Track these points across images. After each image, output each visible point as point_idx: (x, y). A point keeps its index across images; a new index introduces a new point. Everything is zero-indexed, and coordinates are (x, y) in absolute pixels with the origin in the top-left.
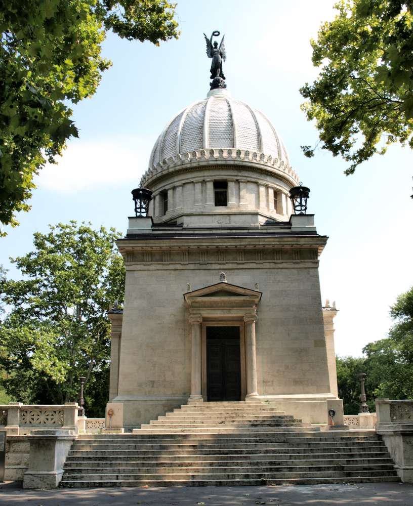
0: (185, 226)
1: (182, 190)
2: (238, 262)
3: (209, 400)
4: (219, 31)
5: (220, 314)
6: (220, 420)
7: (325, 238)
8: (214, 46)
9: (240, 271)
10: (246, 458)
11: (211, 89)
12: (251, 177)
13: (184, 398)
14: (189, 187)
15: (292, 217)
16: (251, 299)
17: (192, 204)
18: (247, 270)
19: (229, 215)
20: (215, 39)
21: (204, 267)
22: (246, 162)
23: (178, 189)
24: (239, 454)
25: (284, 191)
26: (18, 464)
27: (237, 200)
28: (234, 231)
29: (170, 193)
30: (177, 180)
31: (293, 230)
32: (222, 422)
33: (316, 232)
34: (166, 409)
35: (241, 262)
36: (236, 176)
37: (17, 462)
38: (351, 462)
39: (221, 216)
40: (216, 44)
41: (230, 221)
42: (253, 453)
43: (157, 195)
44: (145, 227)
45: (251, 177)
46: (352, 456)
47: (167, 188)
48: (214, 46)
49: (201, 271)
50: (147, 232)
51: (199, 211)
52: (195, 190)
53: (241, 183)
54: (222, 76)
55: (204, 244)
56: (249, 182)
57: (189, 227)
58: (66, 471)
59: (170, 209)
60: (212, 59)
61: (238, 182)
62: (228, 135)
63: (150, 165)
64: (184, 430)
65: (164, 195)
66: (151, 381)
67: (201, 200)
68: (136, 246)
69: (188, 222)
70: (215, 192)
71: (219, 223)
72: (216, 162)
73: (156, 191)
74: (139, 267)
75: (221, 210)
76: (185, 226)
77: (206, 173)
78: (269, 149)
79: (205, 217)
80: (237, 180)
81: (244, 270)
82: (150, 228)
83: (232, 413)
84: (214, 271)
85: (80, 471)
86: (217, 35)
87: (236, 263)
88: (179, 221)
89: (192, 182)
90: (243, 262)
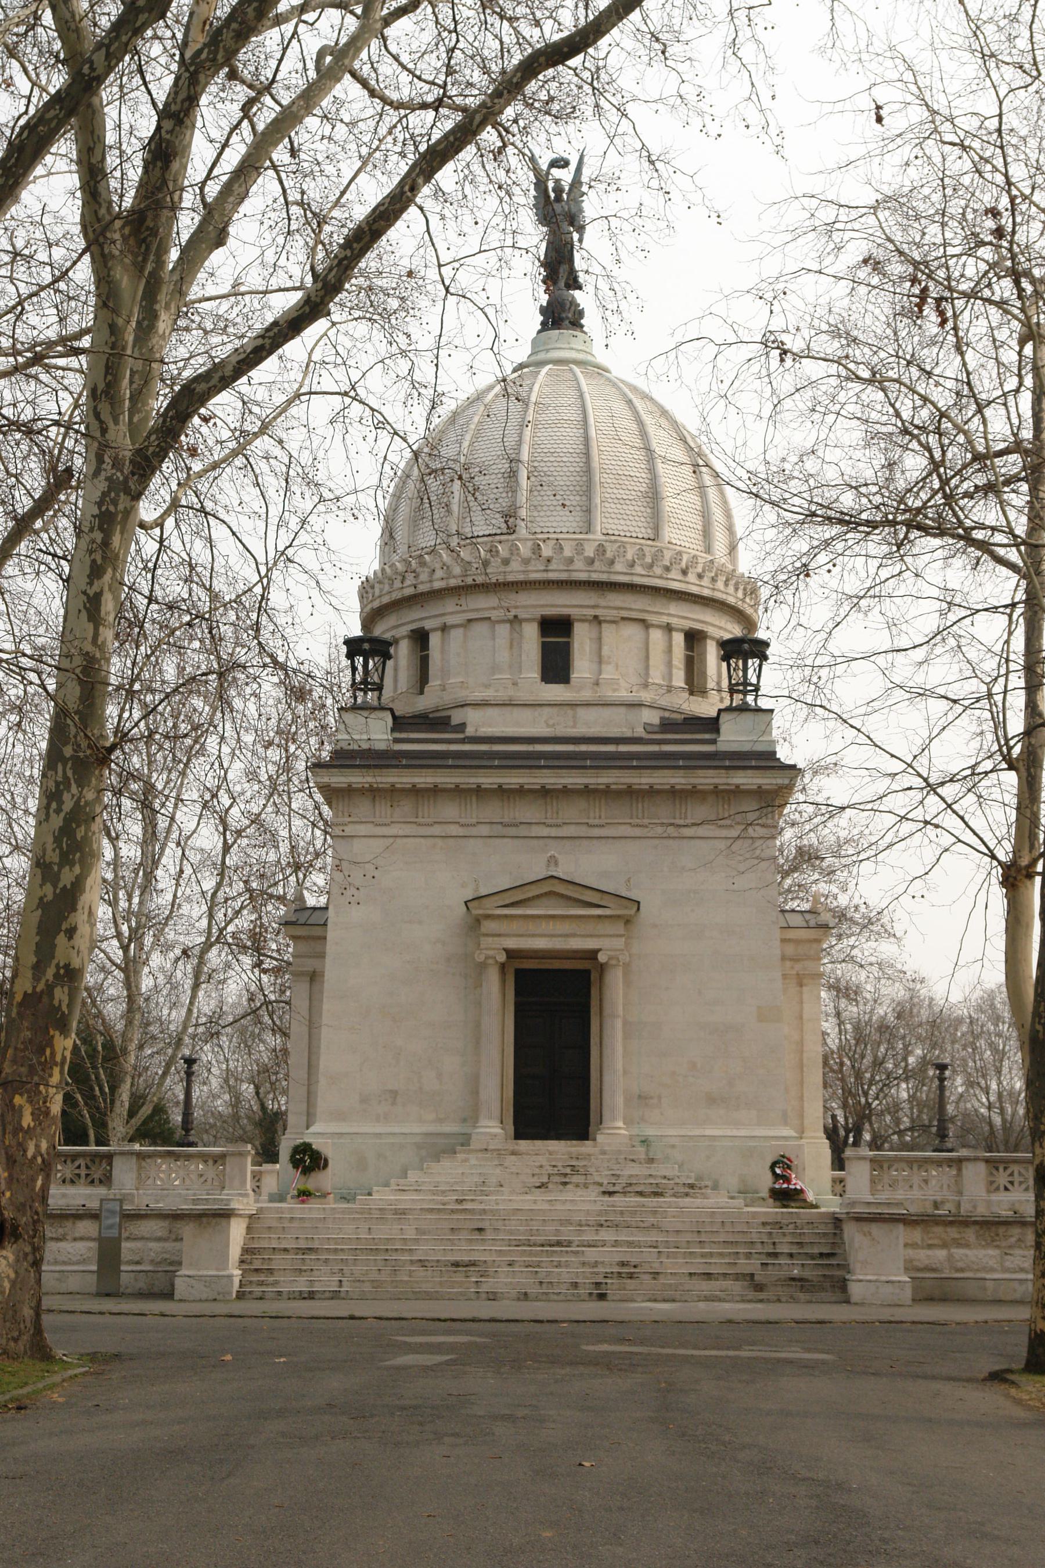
0: (470, 731)
1: (465, 636)
2: (590, 821)
3: (519, 1135)
5: (548, 936)
8: (552, 195)
9: (595, 842)
10: (576, 1253)
11: (545, 326)
12: (631, 609)
13: (463, 1131)
14: (480, 629)
15: (722, 714)
17: (486, 674)
19: (573, 705)
21: (512, 831)
26: (138, 1263)
27: (595, 666)
28: (583, 748)
29: (434, 640)
30: (451, 611)
31: (721, 747)
33: (775, 753)
34: (424, 1153)
35: (597, 822)
37: (137, 1258)
38: (770, 1267)
39: (555, 710)
40: (558, 190)
41: (575, 722)
43: (403, 637)
44: (377, 732)
45: (631, 609)
46: (775, 1255)
48: (552, 195)
49: (506, 840)
50: (382, 746)
51: (502, 695)
52: (494, 639)
57: (478, 734)
58: (244, 1271)
59: (434, 682)
61: (597, 620)
62: (578, 498)
64: (462, 1201)
65: (421, 638)
66: (391, 1091)
67: (510, 667)
69: (480, 723)
70: (544, 645)
71: (548, 726)
74: (362, 829)
75: (555, 692)
76: (470, 731)
78: (681, 533)
79: (516, 710)
80: (596, 617)
81: (603, 841)
84: (535, 842)
85: (271, 1271)
88: (457, 717)
90: (603, 821)
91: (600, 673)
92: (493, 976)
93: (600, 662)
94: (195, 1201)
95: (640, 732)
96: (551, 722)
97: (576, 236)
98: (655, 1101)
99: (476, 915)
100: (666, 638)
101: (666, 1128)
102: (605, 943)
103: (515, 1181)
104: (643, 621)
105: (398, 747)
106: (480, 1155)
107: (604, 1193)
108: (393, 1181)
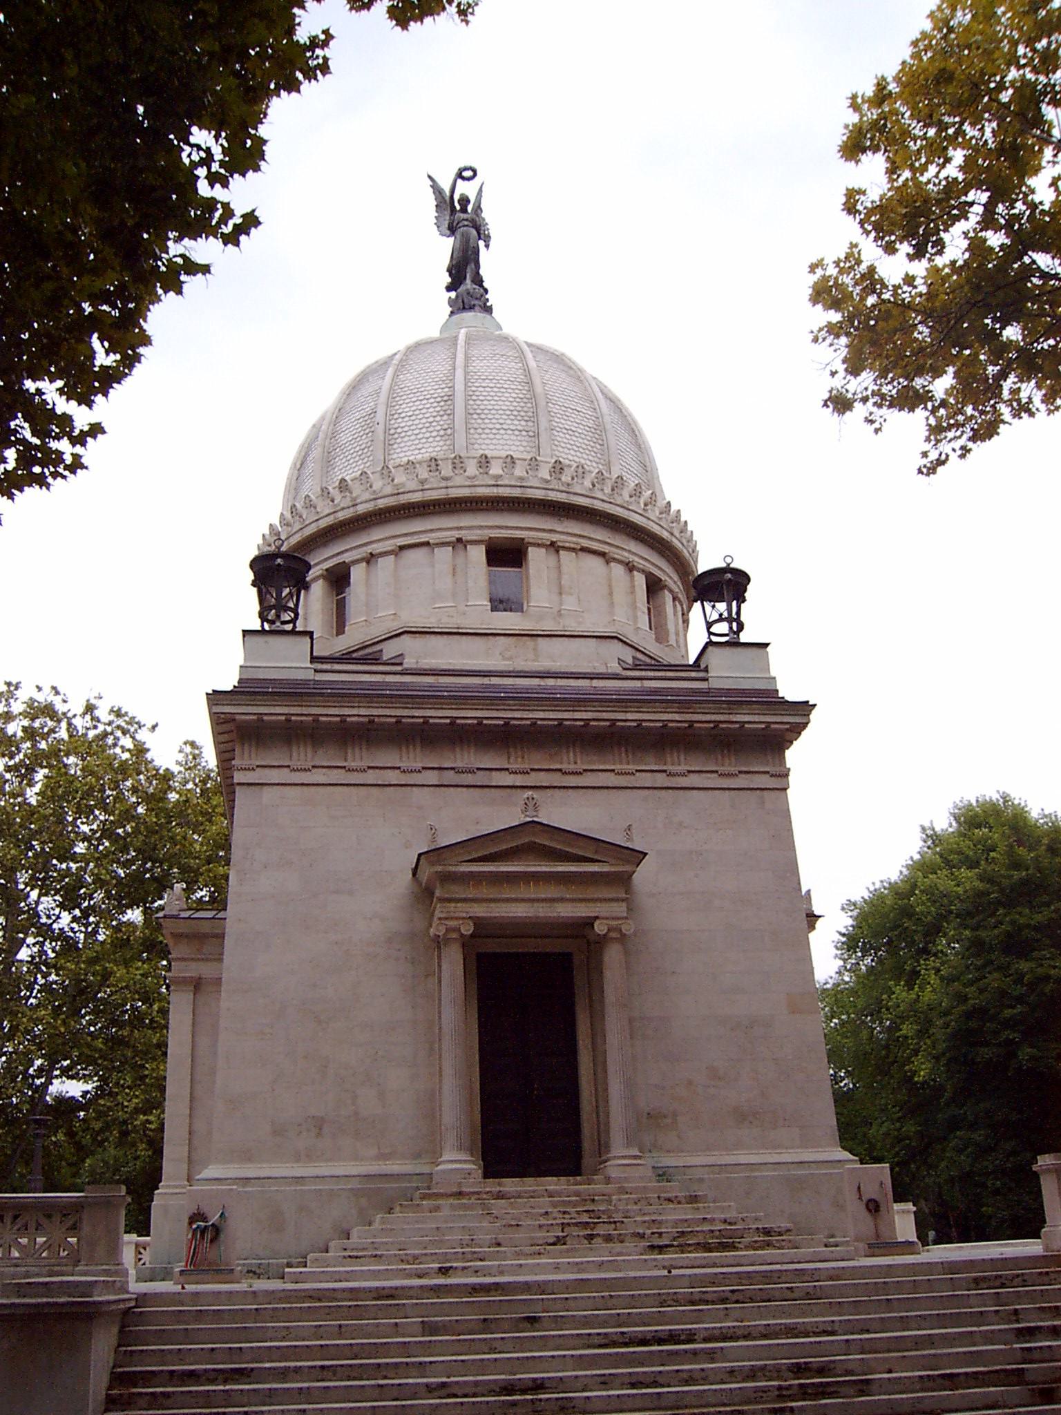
1: (368, 572)
3: (490, 1172)
4: (473, 165)
6: (551, 1236)
7: (805, 708)
8: (458, 207)
15: (710, 648)
16: (616, 865)
18: (591, 791)
20: (463, 188)
21: (468, 779)
22: (575, 494)
23: (381, 561)
24: (683, 1342)
25: (670, 583)
29: (357, 573)
30: (380, 538)
31: (714, 684)
32: (559, 1241)
35: (572, 767)
36: (551, 531)
42: (731, 1339)
44: (290, 661)
47: (347, 558)
48: (458, 207)
50: (301, 675)
52: (433, 566)
53: (561, 552)
54: (478, 281)
55: (470, 715)
56: (583, 549)
60: (452, 239)
61: (554, 547)
62: (523, 423)
63: (286, 500)
65: (339, 579)
68: (250, 720)
69: (417, 653)
71: (504, 659)
72: (495, 490)
73: (321, 562)
76: (409, 663)
77: (466, 520)
80: (553, 544)
82: (309, 665)
83: (578, 1213)
86: (469, 179)
87: (560, 770)
88: (389, 650)
89: (428, 544)
91: (561, 604)
92: (453, 965)
93: (561, 594)
94: (20, 1289)
95: (615, 667)
96: (508, 654)
97: (481, 243)
98: (669, 1121)
99: (437, 873)
100: (628, 578)
101: (693, 1157)
102: (603, 911)
103: (517, 1237)
104: (602, 554)
105: (319, 677)
106: (451, 1201)
107: (652, 1247)
108: (332, 1244)
